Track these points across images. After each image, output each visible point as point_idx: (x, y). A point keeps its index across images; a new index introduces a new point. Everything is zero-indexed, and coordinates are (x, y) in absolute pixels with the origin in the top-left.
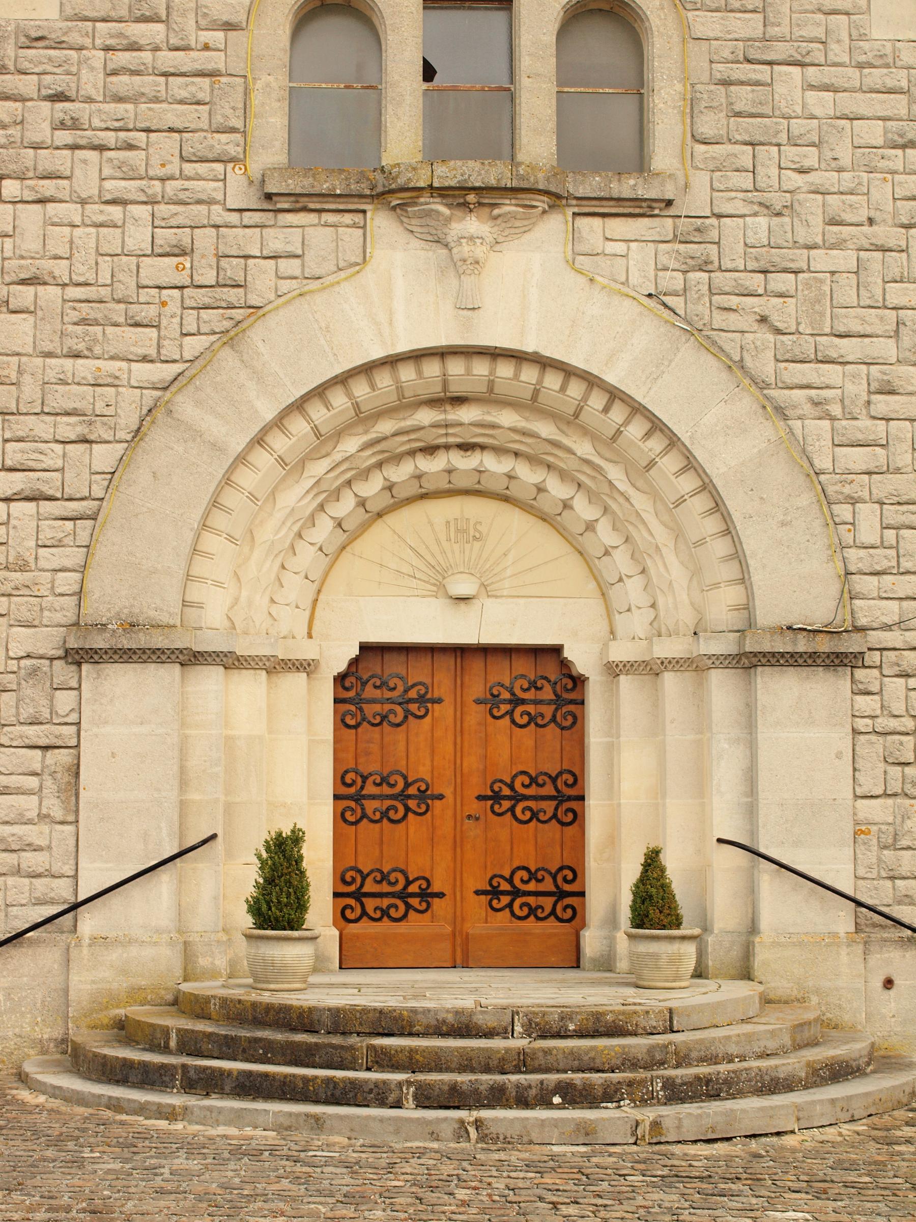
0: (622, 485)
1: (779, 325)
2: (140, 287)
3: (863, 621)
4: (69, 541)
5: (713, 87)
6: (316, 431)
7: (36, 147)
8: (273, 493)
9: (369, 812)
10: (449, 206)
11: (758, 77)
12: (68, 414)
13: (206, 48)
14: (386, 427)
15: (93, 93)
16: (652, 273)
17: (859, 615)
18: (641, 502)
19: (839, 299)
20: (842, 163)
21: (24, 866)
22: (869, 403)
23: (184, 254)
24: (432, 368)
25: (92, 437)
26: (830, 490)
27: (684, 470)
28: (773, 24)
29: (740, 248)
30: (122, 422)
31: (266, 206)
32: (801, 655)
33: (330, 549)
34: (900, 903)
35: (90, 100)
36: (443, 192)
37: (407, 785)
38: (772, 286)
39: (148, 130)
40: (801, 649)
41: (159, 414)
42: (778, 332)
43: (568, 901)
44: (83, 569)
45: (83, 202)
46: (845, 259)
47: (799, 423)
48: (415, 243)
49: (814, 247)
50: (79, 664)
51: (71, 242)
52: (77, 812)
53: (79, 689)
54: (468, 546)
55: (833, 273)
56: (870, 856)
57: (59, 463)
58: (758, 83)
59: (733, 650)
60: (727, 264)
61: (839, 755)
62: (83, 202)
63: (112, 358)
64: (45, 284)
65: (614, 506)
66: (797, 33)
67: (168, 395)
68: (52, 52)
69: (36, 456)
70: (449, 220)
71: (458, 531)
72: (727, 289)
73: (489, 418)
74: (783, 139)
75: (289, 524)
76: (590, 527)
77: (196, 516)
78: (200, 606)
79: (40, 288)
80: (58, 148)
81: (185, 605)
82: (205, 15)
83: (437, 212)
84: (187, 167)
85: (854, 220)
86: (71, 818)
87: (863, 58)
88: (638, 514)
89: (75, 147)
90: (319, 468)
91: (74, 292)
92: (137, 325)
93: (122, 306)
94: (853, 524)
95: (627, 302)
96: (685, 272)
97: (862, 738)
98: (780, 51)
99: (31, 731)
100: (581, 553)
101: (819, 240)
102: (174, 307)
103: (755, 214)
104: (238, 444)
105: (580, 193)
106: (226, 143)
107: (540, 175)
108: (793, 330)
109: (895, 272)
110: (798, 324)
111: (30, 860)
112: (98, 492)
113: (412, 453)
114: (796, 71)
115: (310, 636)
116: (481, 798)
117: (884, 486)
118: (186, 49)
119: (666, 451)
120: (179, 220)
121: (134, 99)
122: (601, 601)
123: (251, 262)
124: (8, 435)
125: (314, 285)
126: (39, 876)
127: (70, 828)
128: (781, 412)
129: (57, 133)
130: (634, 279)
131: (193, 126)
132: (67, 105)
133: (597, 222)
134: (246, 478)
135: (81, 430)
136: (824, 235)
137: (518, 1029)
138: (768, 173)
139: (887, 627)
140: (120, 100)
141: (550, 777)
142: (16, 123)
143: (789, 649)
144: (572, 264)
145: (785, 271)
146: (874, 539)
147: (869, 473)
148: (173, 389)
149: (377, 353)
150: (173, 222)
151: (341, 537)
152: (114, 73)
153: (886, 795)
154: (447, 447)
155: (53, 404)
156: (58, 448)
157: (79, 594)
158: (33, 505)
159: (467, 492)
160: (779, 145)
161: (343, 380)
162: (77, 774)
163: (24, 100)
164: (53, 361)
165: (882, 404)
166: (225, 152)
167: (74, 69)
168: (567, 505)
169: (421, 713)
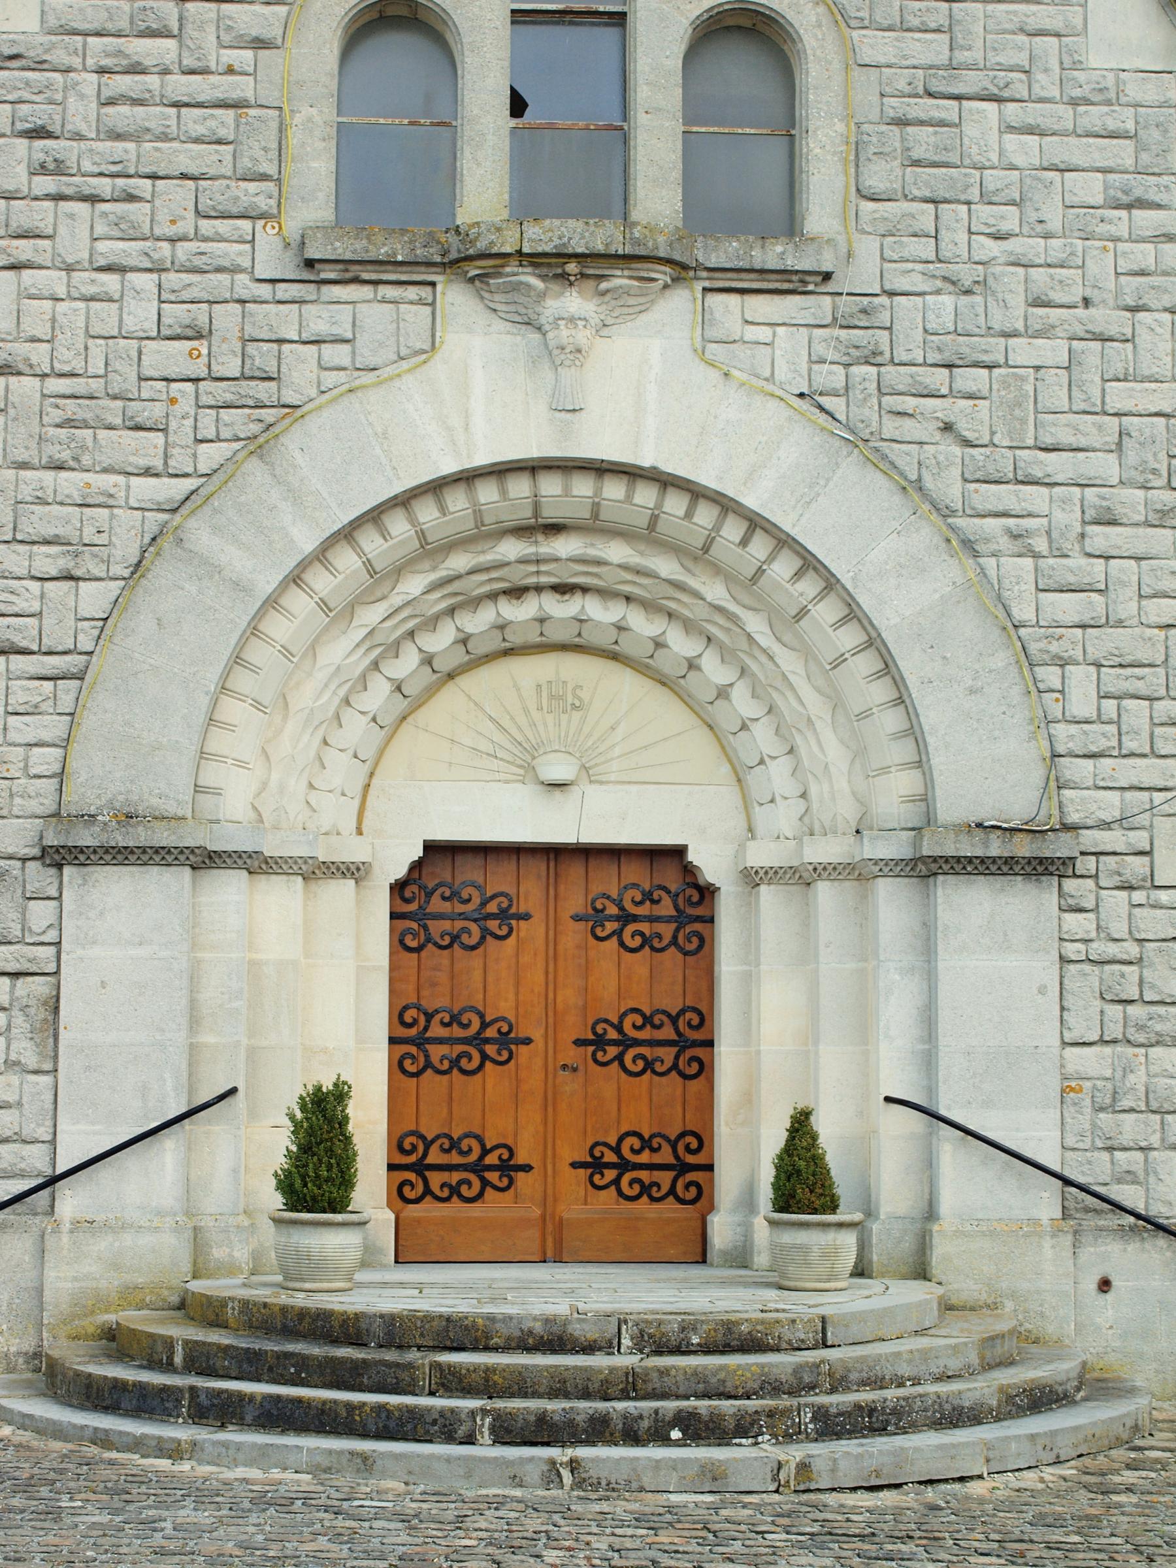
0: (765, 640)
3: (1074, 818)
4: (47, 706)
5: (884, 128)
9: (435, 1060)
10: (543, 278)
13: (230, 71)
14: (459, 562)
17: (1069, 809)
19: (1046, 402)
22: (1083, 535)
23: (199, 336)
24: (520, 487)
25: (78, 573)
26: (1033, 648)
28: (962, 48)
29: (919, 335)
30: (118, 553)
32: (994, 860)
33: (387, 720)
34: (1119, 1181)
35: (79, 137)
36: (535, 260)
37: (484, 1025)
38: (959, 384)
39: (154, 177)
41: (166, 543)
42: (967, 443)
44: (65, 743)
45: (69, 269)
46: (1053, 351)
47: (993, 561)
48: (499, 325)
49: (1014, 334)
50: (59, 866)
51: (53, 320)
52: (56, 1057)
53: (59, 898)
54: (564, 717)
55: (1037, 368)
56: (1082, 1119)
57: (36, 607)
58: (942, 123)
59: (906, 853)
60: (901, 355)
61: (1042, 990)
62: (69, 269)
63: (105, 470)
64: (19, 373)
65: (754, 667)
66: (993, 59)
70: (542, 295)
71: (551, 697)
72: (901, 388)
74: (975, 194)
75: (333, 687)
76: (723, 693)
78: (217, 792)
80: (36, 199)
83: (528, 285)
84: (204, 224)
85: (1065, 300)
86: (48, 1066)
87: (1077, 93)
89: (59, 197)
90: (372, 615)
91: (56, 385)
92: (138, 428)
94: (1062, 692)
97: (1072, 967)
98: (970, 82)
100: (711, 727)
101: (1020, 325)
102: (186, 405)
103: (938, 292)
104: (267, 583)
107: (661, 239)
108: (986, 441)
110: (993, 433)
112: (86, 644)
113: (493, 596)
114: (991, 107)
115: (360, 832)
116: (579, 1043)
117: (1102, 643)
118: (205, 72)
121: (135, 136)
122: (737, 789)
123: (286, 347)
125: (368, 378)
127: (46, 1080)
128: (969, 546)
130: (781, 374)
131: (212, 172)
133: (734, 300)
134: (278, 627)
136: (1026, 319)
137: (626, 1342)
138: (955, 240)
139: (1105, 825)
140: (118, 137)
143: (979, 852)
144: (701, 354)
145: (976, 365)
147: (1083, 626)
148: (184, 511)
149: (449, 467)
150: (185, 295)
151: (402, 705)
152: (111, 102)
153: (1103, 1041)
156: (35, 586)
157: (61, 775)
159: (564, 647)
160: (968, 203)
161: (404, 501)
162: (56, 1010)
165: (1101, 538)
166: (254, 206)
167: (59, 97)
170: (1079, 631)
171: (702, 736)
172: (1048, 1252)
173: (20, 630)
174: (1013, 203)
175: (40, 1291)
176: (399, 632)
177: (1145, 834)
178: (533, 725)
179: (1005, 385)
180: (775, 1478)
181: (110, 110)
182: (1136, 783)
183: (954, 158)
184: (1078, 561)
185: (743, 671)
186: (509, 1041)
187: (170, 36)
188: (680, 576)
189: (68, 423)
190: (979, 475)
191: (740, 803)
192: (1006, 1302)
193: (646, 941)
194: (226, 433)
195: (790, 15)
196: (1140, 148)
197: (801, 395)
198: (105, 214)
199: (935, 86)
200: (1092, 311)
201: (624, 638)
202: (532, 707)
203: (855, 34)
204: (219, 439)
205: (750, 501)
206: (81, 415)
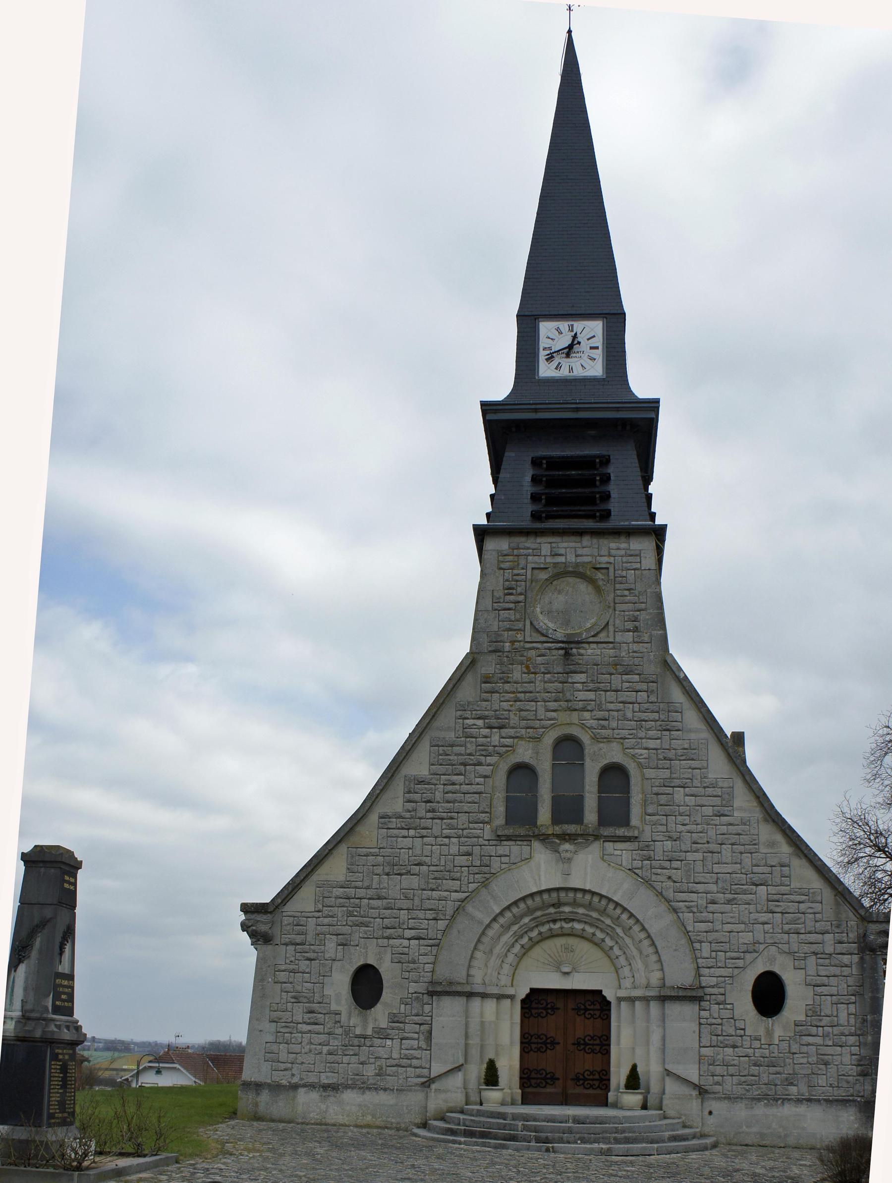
0: (621, 934)
1: (676, 880)
2: (454, 866)
3: (703, 985)
4: (429, 953)
5: (653, 796)
6: (514, 916)
7: (420, 818)
8: (499, 936)
9: (533, 1048)
10: (560, 840)
11: (667, 792)
12: (430, 910)
13: (478, 784)
14: (539, 913)
15: (439, 800)
16: (630, 861)
17: (702, 982)
18: (628, 941)
19: (696, 870)
20: (697, 822)
21: (412, 1064)
22: (707, 907)
23: (469, 855)
24: (554, 895)
25: (438, 918)
26: (692, 938)
27: (641, 930)
28: (673, 773)
29: (661, 852)
30: (448, 913)
31: (497, 839)
32: (680, 996)
33: (519, 955)
34: (715, 1085)
35: (438, 802)
36: (557, 836)
37: (547, 1039)
38: (673, 866)
39: (458, 813)
40: (681, 995)
41: (460, 910)
42: (675, 882)
43: (604, 1082)
44: (434, 963)
45: (436, 837)
46: (699, 856)
47: (681, 914)
48: (548, 851)
49: (688, 852)
50: (432, 996)
51: (432, 851)
52: (431, 1046)
53: (432, 1004)
54: (568, 954)
55: (694, 861)
56: (704, 1067)
57: (427, 927)
58: (668, 794)
59: (657, 994)
60: (657, 858)
61: (694, 1032)
62: (436, 837)
63: (445, 891)
64: (423, 865)
65: (619, 942)
66: (682, 776)
67: (464, 904)
68: (426, 786)
69: (418, 924)
70: (560, 844)
71: (565, 949)
72: (657, 867)
73: (574, 910)
74: (677, 813)
75: (505, 947)
76: (611, 948)
77: (472, 945)
78: (473, 976)
79: (421, 867)
80: (427, 819)
81: (468, 975)
82: (478, 773)
83: (555, 842)
84: (470, 825)
85: (702, 842)
86: (429, 1048)
87: (705, 785)
88: (627, 944)
89: (433, 819)
90: (515, 928)
91: (432, 868)
92: (453, 880)
93: (448, 873)
94: (700, 950)
95: (622, 872)
96: (642, 861)
97: (703, 1026)
98: (677, 782)
99: (416, 1018)
100: (609, 957)
101: (689, 849)
102: (465, 874)
103: (667, 840)
104: (487, 921)
105: (605, 834)
106: (483, 816)
107: (590, 829)
108: (680, 881)
109: (716, 860)
110: (682, 879)
111: (415, 1062)
112: (439, 937)
113: (548, 922)
114: (682, 789)
115: (512, 986)
116: (573, 1044)
117: (712, 936)
118: (471, 784)
119: (636, 923)
120: (468, 843)
121: (454, 802)
122: (616, 974)
123: (492, 858)
124: (409, 917)
125: (514, 866)
126: (418, 1068)
127: (428, 1052)
128: (675, 911)
129: (428, 814)
130: (624, 864)
131: (473, 811)
132: (431, 804)
133: (611, 844)
134: (490, 933)
135: (434, 916)
136: (691, 847)
137: (570, 1121)
138: (671, 826)
139: (713, 987)
140: (449, 802)
141: (598, 1037)
142: (413, 810)
143: (676, 994)
144: (602, 859)
145: (677, 860)
146: (707, 955)
147: (707, 932)
148: (466, 902)
149: (535, 890)
150: (466, 844)
151: (523, 951)
152: (447, 793)
153: (711, 1046)
154: (561, 920)
155: (425, 906)
156: (426, 921)
157: (432, 972)
158: (418, 941)
159: (569, 935)
160: (675, 816)
161: (523, 899)
162: (431, 1034)
163: (416, 802)
164: (425, 892)
165: (712, 907)
166: (483, 820)
167: (433, 792)
168: (603, 940)
169: (552, 1013)
170: (705, 933)
171: (606, 959)
172: (694, 1104)
173: (422, 933)
174: (687, 816)
175: (426, 1107)
176: (523, 932)
177: (723, 989)
178: (560, 956)
179: (685, 865)
180: (601, 1152)
181: (447, 795)
182: (720, 975)
183: (671, 803)
184: (705, 914)
185: (617, 943)
186: (554, 1043)
187: (462, 775)
188: (599, 917)
189: (435, 878)
190: (678, 890)
191: (617, 977)
192: (682, 1116)
193: (592, 1016)
194: (476, 881)
195: (627, 766)
196: (723, 800)
197: (629, 869)
198: (445, 823)
199: (667, 784)
200: (709, 845)
201: (584, 933)
202: (560, 951)
203: (645, 770)
204: (474, 882)
205: (615, 899)
206: (438, 876)
